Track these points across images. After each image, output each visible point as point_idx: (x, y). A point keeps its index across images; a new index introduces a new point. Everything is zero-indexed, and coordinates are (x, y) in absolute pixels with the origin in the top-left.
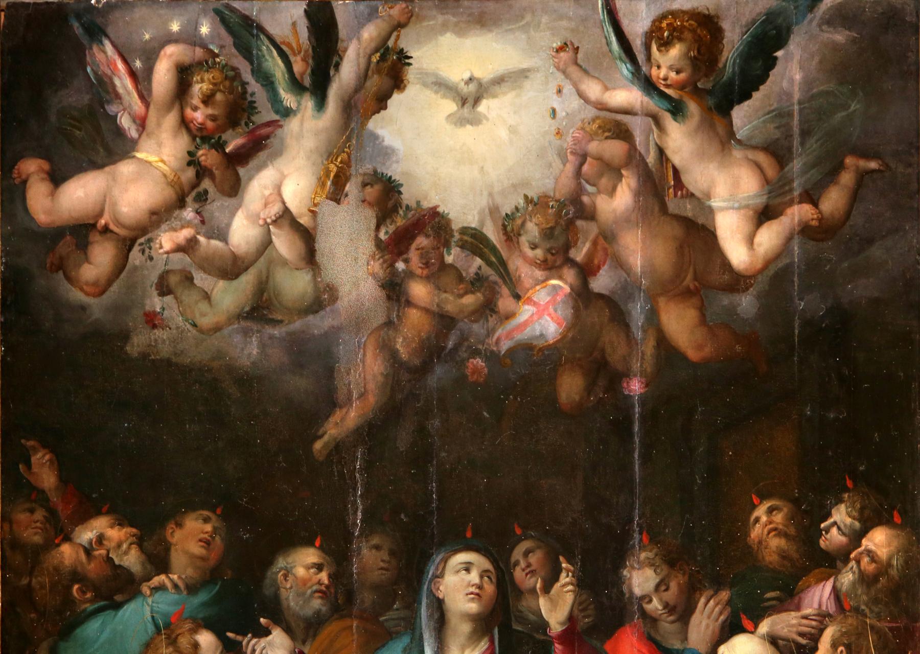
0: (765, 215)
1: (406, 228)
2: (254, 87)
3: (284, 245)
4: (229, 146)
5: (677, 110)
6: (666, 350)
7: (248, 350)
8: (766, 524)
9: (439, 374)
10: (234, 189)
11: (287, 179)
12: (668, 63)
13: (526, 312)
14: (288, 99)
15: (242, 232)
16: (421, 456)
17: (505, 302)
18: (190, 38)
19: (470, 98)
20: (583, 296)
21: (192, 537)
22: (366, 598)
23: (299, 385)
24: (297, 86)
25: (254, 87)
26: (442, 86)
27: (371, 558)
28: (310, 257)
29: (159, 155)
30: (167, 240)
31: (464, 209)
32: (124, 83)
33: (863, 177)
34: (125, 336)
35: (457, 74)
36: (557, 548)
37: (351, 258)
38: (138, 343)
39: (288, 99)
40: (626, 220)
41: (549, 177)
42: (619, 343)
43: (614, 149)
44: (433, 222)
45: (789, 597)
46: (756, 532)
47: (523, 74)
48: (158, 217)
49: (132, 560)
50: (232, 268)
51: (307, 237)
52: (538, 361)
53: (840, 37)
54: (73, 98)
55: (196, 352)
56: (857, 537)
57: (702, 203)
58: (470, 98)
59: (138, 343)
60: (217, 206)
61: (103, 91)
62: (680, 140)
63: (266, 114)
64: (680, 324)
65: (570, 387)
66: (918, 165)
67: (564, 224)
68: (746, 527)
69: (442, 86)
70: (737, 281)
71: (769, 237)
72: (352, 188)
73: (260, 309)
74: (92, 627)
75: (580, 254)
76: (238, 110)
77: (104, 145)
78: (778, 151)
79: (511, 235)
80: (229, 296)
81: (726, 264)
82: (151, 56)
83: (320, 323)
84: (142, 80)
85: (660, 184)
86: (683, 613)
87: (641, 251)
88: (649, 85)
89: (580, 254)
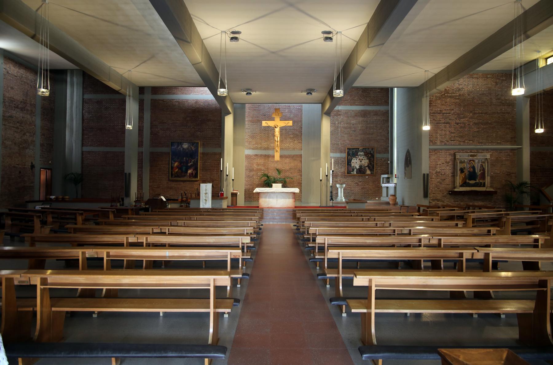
1: (183, 149)
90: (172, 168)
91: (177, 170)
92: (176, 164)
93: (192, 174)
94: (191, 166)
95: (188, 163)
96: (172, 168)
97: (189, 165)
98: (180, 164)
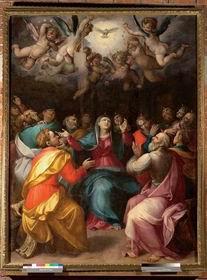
0: (166, 55)
1: (93, 57)
2: (62, 31)
3: (67, 60)
4: (56, 42)
5: (148, 35)
6: (146, 80)
7: (59, 79)
8: (166, 113)
9: (99, 83)
10: (57, 50)
11: (68, 48)
12: (146, 27)
13: (117, 73)
14: (68, 33)
15: (59, 58)
16: (96, 98)
17: (113, 71)
18: (47, 22)
19: (106, 33)
20: (129, 70)
21: (48, 114)
22: (84, 125)
23: (72, 86)
24: (70, 31)
25: (62, 31)
26: (100, 31)
27: (86, 118)
28: (73, 62)
29: (42, 44)
30: (43, 59)
31: (104, 53)
32: (34, 30)
33: (185, 48)
34: (34, 77)
35: (103, 29)
36: (123, 116)
37: (81, 60)
38: (37, 79)
39: (68, 33)
40: (137, 56)
41: (122, 48)
42: (30, 245)
43: (135, 42)
44: (98, 56)
45: (170, 125)
46: (164, 114)
47: (117, 29)
48: (41, 55)
49: (36, 118)
50: (56, 65)
51: (72, 59)
52: (118, 83)
53: (181, 22)
54: (23, 33)
55: (49, 80)
56: (184, 115)
57: (153, 53)
58: (106, 33)
59: (37, 79)
60: (53, 53)
61: (30, 32)
62: (149, 41)
63: (63, 36)
64: (149, 75)
65: (126, 87)
66: (15, 236)
67: (126, 55)
68: (161, 113)
69: (100, 31)
70: (161, 68)
71: (166, 59)
72: (81, 49)
73: (62, 72)
74: (27, 130)
75: (128, 62)
76: (58, 36)
77: (31, 42)
78: (169, 44)
79: (114, 58)
80: (56, 70)
81: (158, 64)
82: (40, 26)
83: (76, 74)
84: (38, 30)
85: (144, 49)
86: (149, 129)
87: (141, 61)
88: (142, 31)
89: (128, 62)
90: (15, 188)
91: (52, 203)
92: (48, 162)
93: (158, 228)
94: (151, 173)
95: (129, 154)
96: (15, 188)
97: (138, 164)
98: (77, 160)
